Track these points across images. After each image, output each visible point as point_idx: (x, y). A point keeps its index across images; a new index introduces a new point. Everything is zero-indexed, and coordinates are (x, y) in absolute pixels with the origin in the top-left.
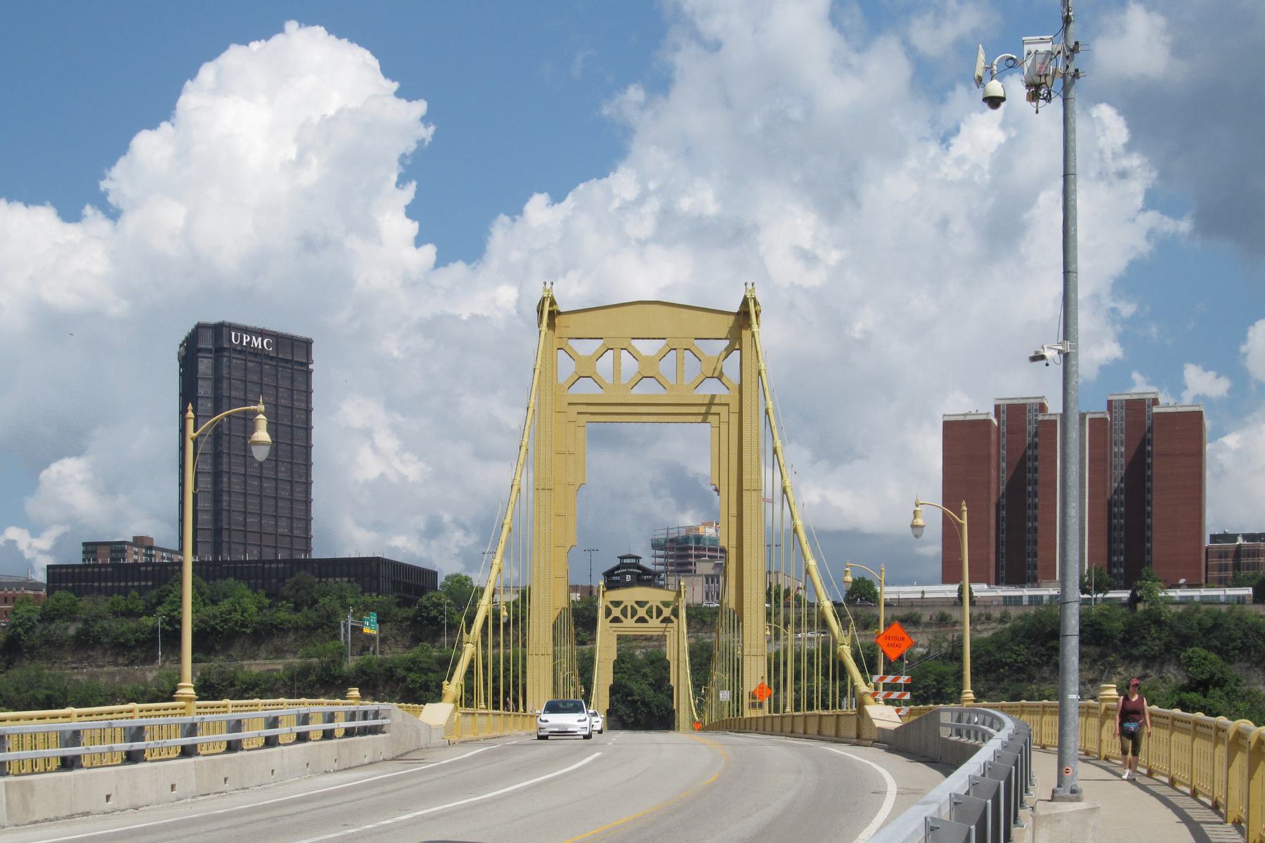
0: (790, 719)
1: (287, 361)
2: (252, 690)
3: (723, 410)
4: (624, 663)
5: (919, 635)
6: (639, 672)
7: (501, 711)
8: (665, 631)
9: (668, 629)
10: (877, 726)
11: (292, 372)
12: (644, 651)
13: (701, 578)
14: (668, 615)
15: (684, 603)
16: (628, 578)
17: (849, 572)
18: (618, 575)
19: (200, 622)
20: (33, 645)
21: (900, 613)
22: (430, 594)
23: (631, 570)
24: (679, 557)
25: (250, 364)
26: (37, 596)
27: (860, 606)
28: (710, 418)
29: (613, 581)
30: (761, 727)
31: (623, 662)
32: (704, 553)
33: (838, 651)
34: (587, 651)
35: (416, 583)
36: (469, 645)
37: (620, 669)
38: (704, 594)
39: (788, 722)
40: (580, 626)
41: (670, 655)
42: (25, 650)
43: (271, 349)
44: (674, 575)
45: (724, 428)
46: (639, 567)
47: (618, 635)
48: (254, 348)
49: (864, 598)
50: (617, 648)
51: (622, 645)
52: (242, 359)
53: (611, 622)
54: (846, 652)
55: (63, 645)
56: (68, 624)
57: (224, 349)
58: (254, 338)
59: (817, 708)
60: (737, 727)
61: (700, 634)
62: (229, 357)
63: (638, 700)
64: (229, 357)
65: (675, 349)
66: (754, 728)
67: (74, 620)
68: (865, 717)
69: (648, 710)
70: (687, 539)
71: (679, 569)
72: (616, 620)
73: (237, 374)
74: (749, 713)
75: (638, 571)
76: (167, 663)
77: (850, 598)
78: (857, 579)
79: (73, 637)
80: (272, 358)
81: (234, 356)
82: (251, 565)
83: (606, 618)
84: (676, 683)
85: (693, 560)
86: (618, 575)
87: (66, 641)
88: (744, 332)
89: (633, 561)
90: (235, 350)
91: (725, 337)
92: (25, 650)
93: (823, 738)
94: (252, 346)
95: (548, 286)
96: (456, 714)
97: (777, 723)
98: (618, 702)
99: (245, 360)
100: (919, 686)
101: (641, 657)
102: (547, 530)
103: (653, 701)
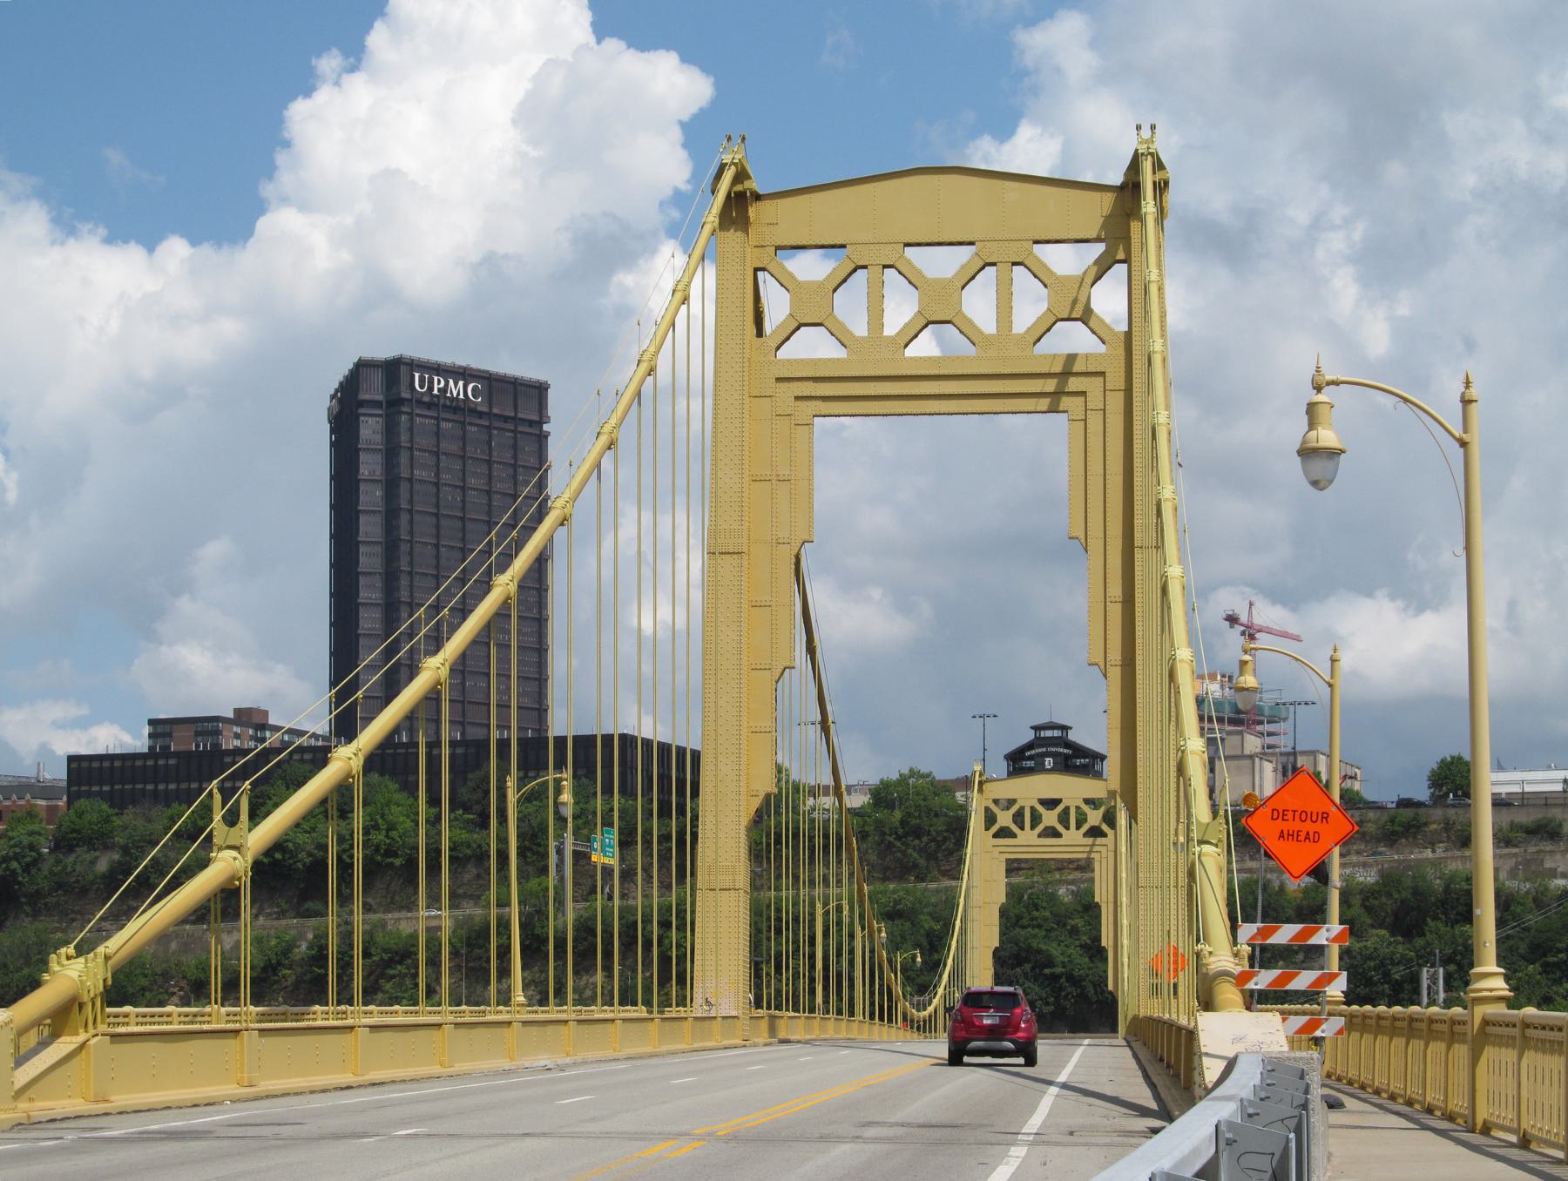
1: (506, 419)
2: (400, 963)
3: (1093, 386)
4: (1037, 910)
5: (1558, 856)
8: (1090, 852)
9: (1096, 849)
11: (515, 438)
12: (1074, 888)
14: (1097, 824)
18: (1031, 758)
19: (316, 848)
20: (37, 890)
21: (1525, 817)
23: (1053, 749)
25: (444, 425)
26: (52, 810)
27: (1453, 806)
28: (1066, 402)
37: (1032, 919)
42: (23, 900)
43: (480, 400)
46: (1069, 744)
47: (1007, 860)
48: (452, 399)
49: (1460, 793)
51: (1035, 879)
52: (432, 417)
53: (995, 836)
55: (87, 890)
56: (97, 854)
57: (401, 401)
58: (451, 381)
62: (410, 414)
63: (1062, 974)
64: (410, 414)
67: (107, 848)
72: (1004, 833)
73: (423, 441)
75: (1065, 751)
76: (261, 918)
78: (1449, 759)
79: (104, 876)
80: (481, 414)
81: (418, 411)
82: (398, 751)
83: (987, 829)
84: (1111, 943)
86: (1031, 758)
87: (93, 882)
89: (1057, 733)
90: (419, 402)
91: (1094, 235)
92: (23, 900)
94: (448, 395)
98: (1027, 979)
99: (437, 419)
100: (1559, 945)
103: (1088, 975)
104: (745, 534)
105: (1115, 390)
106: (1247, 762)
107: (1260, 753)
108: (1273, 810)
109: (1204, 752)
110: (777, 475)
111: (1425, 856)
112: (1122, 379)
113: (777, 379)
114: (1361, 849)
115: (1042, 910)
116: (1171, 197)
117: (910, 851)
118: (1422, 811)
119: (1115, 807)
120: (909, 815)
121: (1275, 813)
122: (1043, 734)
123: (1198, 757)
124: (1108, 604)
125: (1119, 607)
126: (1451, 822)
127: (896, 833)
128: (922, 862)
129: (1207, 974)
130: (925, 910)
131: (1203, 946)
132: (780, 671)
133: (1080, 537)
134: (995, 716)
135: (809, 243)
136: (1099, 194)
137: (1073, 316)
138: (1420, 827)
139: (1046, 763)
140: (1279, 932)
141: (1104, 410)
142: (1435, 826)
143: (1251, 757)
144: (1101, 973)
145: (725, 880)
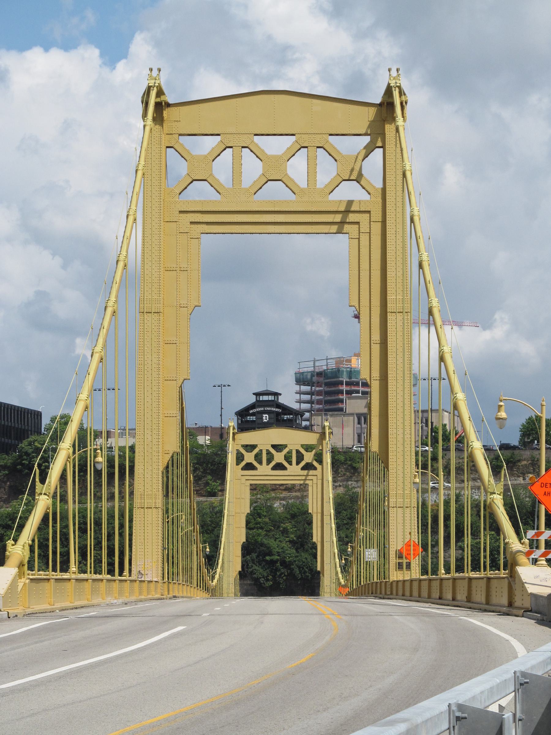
0: (417, 582)
3: (363, 219)
6: (279, 527)
7: (117, 577)
8: (305, 480)
10: (529, 592)
12: (284, 502)
13: (351, 418)
15: (329, 446)
16: (266, 418)
17: (503, 407)
18: (253, 414)
22: (32, 438)
23: (269, 409)
24: (327, 393)
28: (347, 228)
29: (248, 421)
30: (415, 593)
31: (260, 516)
32: (356, 388)
33: (489, 501)
34: (216, 504)
35: (10, 424)
36: (43, 497)
37: (257, 524)
39: (448, 586)
40: (209, 474)
41: (313, 507)
44: (321, 415)
45: (364, 239)
46: (279, 406)
50: (251, 500)
51: (259, 496)
53: (243, 469)
54: (498, 501)
59: (485, 570)
60: (383, 592)
61: (350, 483)
63: (277, 560)
65: (306, 147)
66: (400, 593)
68: (517, 580)
70: (337, 372)
71: (328, 407)
72: (249, 467)
74: (395, 576)
75: (277, 410)
77: (526, 440)
84: (319, 540)
85: (344, 397)
86: (253, 414)
88: (387, 127)
89: (271, 398)
91: (364, 132)
95: (155, 73)
96: (23, 580)
98: (254, 563)
102: (155, 360)
103: (295, 561)
104: (162, 301)
105: (376, 222)
108: (542, 483)
109: (482, 448)
110: (180, 268)
111: (518, 482)
112: (380, 215)
113: (180, 211)
114: (475, 477)
116: (408, 108)
118: (517, 452)
119: (322, 450)
121: (542, 484)
122: (261, 398)
124: (372, 344)
125: (378, 346)
126: (536, 460)
129: (512, 552)
131: (509, 540)
132: (182, 381)
133: (356, 306)
134: (229, 386)
136: (367, 108)
137: (351, 178)
138: (515, 463)
139: (264, 418)
140: (549, 536)
141: (370, 233)
142: (525, 462)
144: (304, 560)
145: (147, 502)
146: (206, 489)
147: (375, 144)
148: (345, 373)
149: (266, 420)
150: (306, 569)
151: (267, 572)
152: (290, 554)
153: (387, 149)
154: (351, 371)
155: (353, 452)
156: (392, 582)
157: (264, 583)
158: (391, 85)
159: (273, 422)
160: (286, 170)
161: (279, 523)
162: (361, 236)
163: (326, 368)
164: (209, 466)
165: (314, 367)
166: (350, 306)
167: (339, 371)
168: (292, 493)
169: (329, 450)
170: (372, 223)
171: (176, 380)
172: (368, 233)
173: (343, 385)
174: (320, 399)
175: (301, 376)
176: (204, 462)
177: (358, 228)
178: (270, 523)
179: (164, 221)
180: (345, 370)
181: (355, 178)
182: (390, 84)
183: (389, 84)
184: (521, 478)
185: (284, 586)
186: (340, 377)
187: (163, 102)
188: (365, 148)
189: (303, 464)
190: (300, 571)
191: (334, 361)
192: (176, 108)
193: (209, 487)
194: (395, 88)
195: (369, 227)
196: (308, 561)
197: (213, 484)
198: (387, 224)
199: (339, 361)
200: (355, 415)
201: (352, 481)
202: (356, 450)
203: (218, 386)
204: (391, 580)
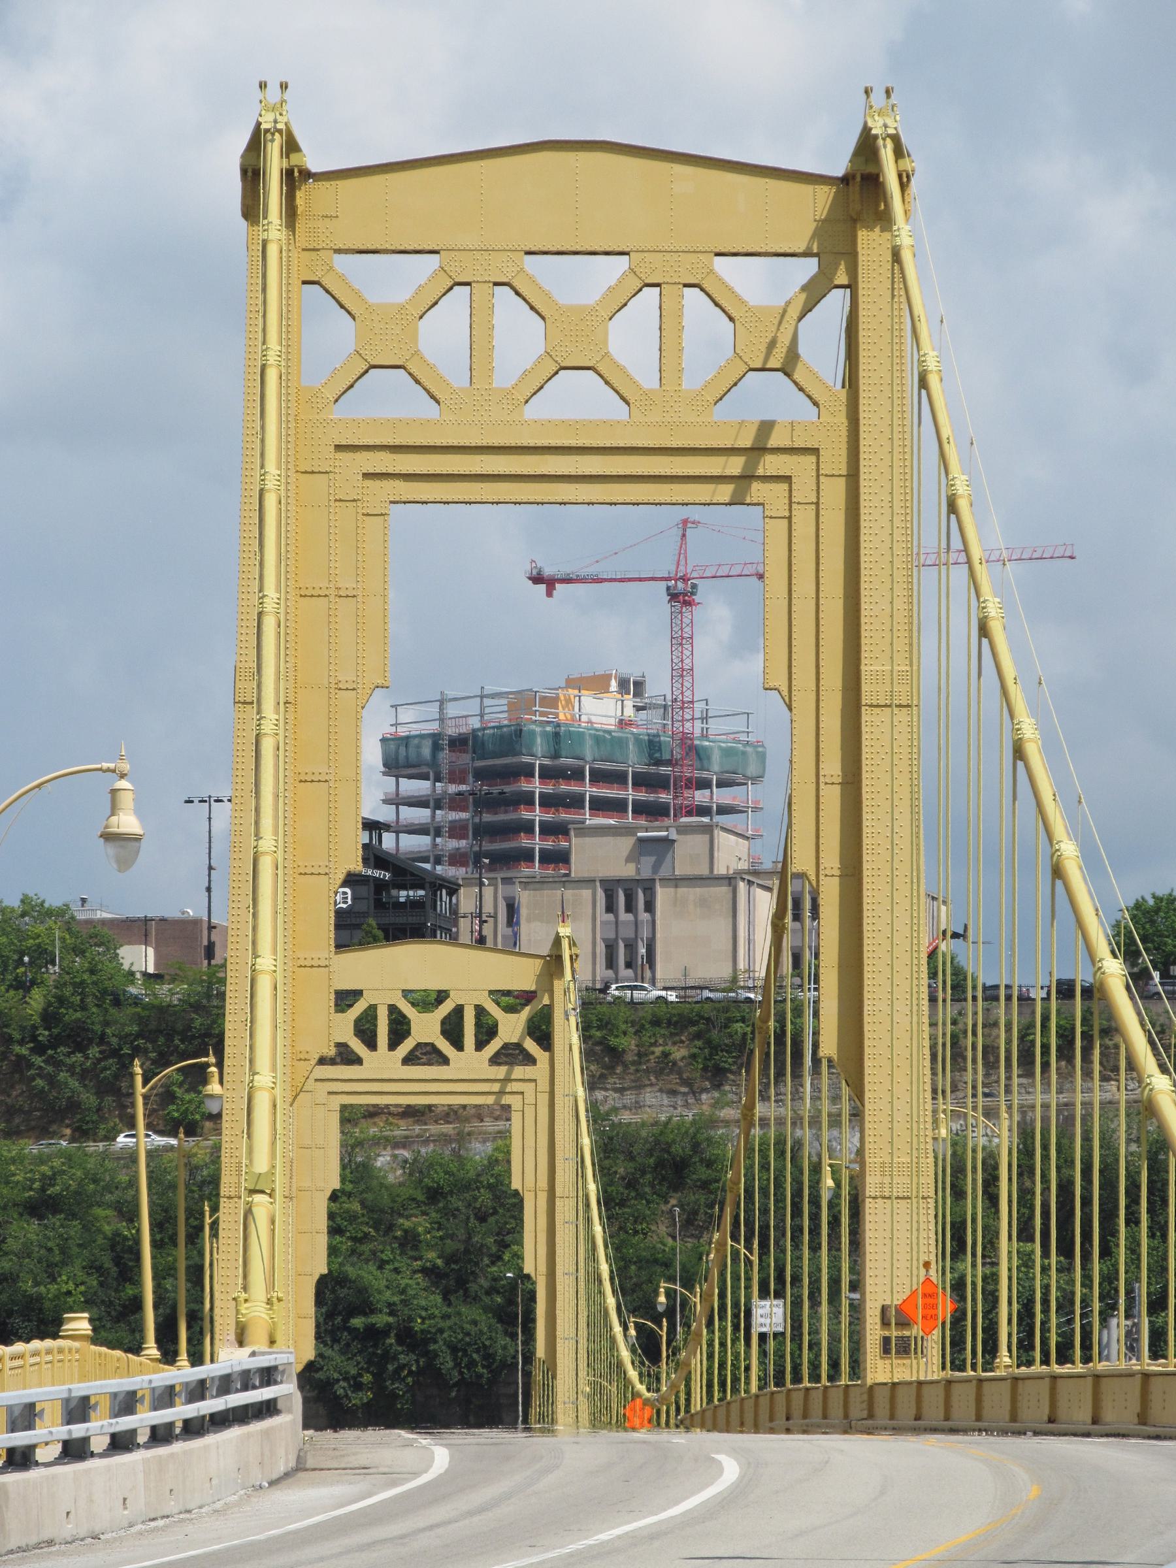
6: (390, 1228)
8: (502, 1093)
12: (406, 1154)
13: (586, 893)
14: (515, 1040)
28: (758, 490)
32: (574, 788)
38: (601, 949)
45: (803, 519)
47: (344, 1108)
63: (389, 1325)
69: (422, 1361)
75: (377, 873)
78: (1151, 902)
84: (542, 1268)
91: (801, 248)
93: (1158, 1430)
95: (273, 94)
97: (963, 1400)
101: (395, 1176)
103: (441, 1331)
105: (833, 476)
106: (723, 890)
107: (749, 872)
113: (337, 446)
115: (344, 1198)
117: (63, 1076)
120: (61, 1000)
123: (1168, 1097)
124: (822, 786)
125: (836, 791)
127: (34, 1038)
128: (88, 1098)
130: (108, 1197)
133: (781, 689)
135: (383, 247)
137: (768, 366)
141: (817, 504)
143: (730, 880)
144: (467, 1326)
146: (166, 1112)
147: (831, 280)
148: (539, 740)
149: (345, 902)
150: (475, 1356)
151: (358, 1363)
152: (426, 1310)
153: (861, 292)
154: (556, 735)
155: (610, 1003)
156: (871, 1387)
157: (346, 1396)
158: (874, 132)
159: (365, 909)
160: (605, 341)
161: (392, 1216)
162: (794, 513)
163: (477, 725)
164: (177, 1042)
165: (442, 720)
166: (766, 689)
167: (519, 733)
168: (426, 1124)
169: (574, 1009)
170: (822, 479)
171: (326, 874)
172: (812, 503)
173: (533, 776)
174: (460, 820)
175: (402, 750)
176: (161, 1032)
177: (787, 492)
178: (363, 1215)
179: (297, 471)
180: (538, 729)
181: (778, 365)
182: (871, 129)
183: (866, 130)
184: (1113, 1083)
185: (406, 1404)
186: (524, 751)
187: (296, 170)
188: (804, 288)
189: (494, 1046)
190: (455, 1360)
191: (505, 701)
192: (327, 184)
193: (175, 1107)
194: (884, 139)
195: (815, 488)
196: (481, 1331)
197: (187, 1097)
198: (862, 483)
199: (523, 700)
200: (598, 884)
201: (606, 1090)
202: (619, 998)
203: (200, 801)
204: (869, 1382)
